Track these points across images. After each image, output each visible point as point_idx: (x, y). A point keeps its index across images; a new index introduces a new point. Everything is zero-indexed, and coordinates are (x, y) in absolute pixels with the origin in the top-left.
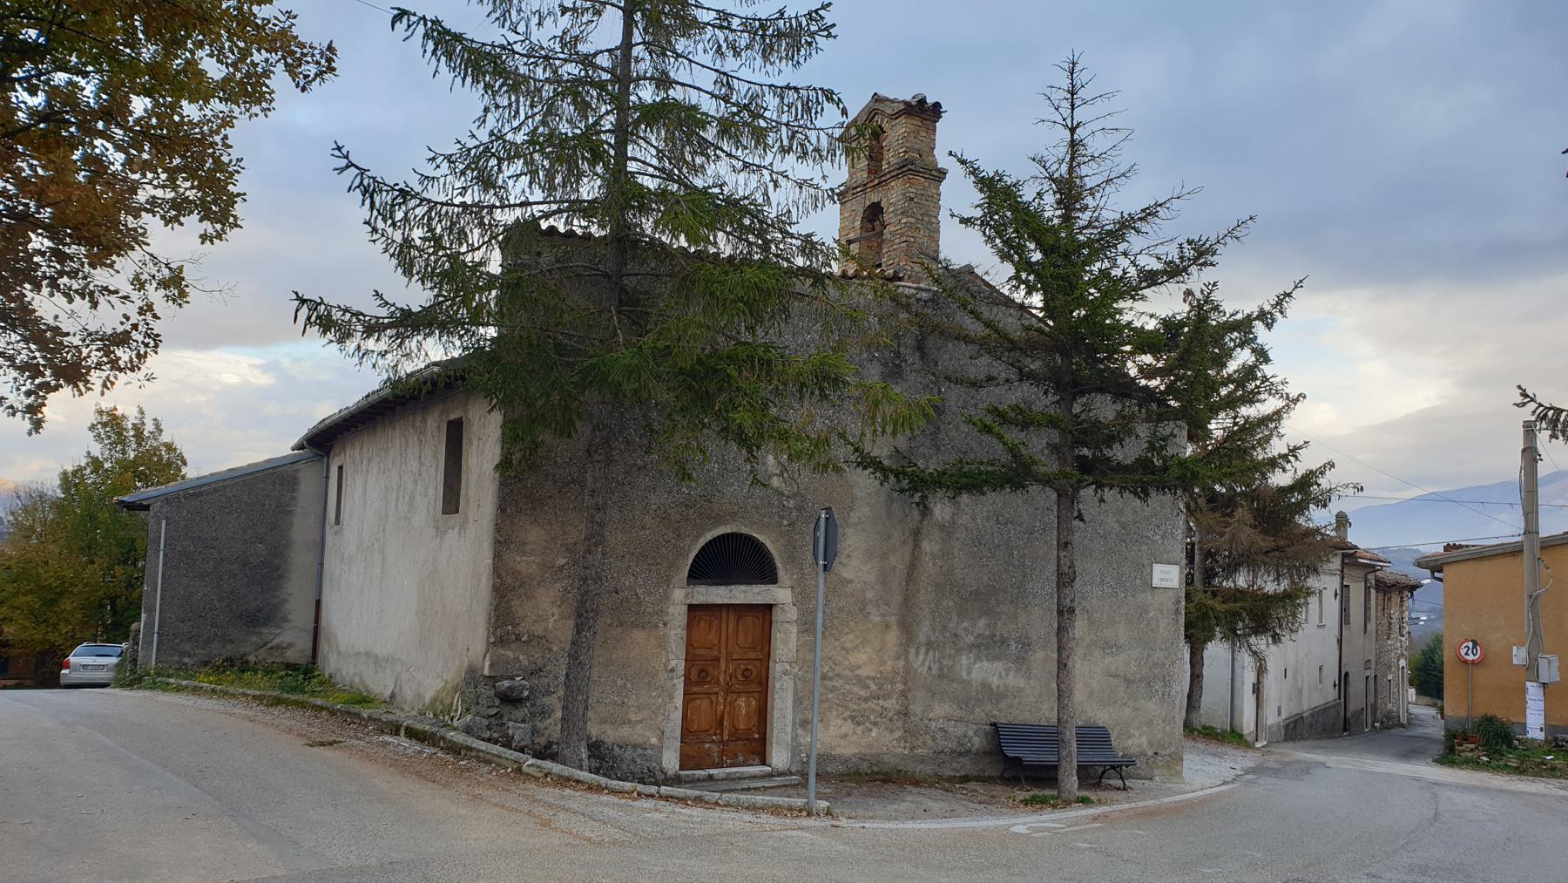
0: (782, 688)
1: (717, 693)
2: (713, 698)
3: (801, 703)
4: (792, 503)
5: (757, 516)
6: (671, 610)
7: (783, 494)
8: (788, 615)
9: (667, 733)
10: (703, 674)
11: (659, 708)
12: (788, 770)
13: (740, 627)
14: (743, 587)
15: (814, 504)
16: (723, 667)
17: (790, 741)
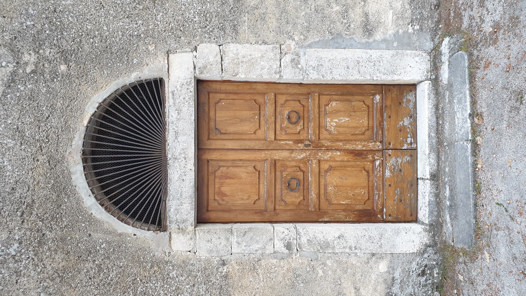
0: (318, 68)
1: (319, 161)
2: (325, 166)
3: (339, 35)
4: (29, 58)
5: (54, 121)
6: (203, 254)
7: (14, 73)
8: (211, 59)
9: (373, 248)
10: (294, 183)
11: (339, 262)
12: (429, 54)
13: (231, 129)
14: (170, 137)
15: (29, 16)
16: (285, 154)
17: (391, 52)
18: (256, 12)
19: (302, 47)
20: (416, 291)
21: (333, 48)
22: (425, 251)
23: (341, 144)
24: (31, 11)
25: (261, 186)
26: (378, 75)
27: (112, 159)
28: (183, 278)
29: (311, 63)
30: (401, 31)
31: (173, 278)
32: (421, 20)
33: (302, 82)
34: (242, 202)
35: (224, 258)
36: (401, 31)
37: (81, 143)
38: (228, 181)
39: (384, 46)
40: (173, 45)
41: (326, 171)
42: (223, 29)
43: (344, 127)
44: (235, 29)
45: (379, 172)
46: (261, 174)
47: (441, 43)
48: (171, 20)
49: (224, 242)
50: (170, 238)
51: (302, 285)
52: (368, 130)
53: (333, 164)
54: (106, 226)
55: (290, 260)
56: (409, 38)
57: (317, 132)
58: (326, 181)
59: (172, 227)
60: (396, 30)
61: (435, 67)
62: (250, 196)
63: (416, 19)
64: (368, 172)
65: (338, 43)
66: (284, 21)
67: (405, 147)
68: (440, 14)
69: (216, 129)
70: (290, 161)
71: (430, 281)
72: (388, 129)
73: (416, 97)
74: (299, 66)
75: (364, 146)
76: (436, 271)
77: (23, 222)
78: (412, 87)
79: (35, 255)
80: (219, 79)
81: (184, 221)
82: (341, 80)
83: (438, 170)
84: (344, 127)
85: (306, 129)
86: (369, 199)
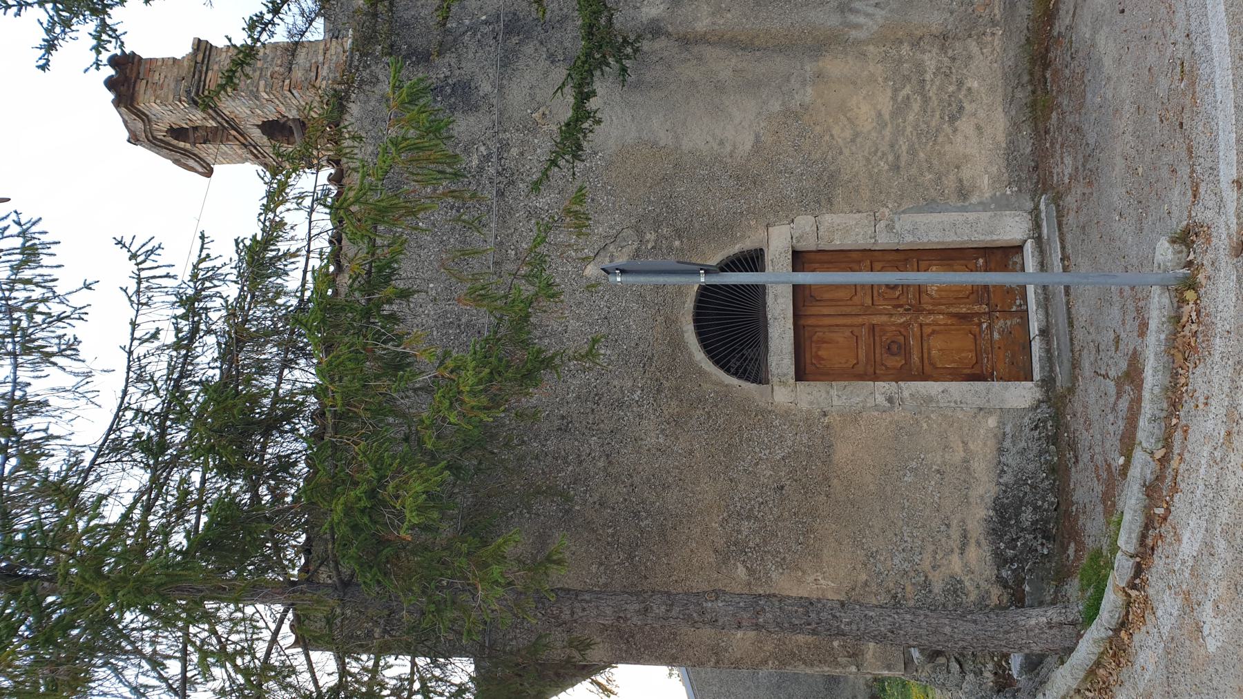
0: (912, 232)
2: (927, 330)
6: (804, 406)
7: (638, 250)
8: (808, 229)
9: (980, 403)
10: (894, 347)
12: (1030, 213)
16: (884, 319)
17: (989, 214)
18: (850, 185)
19: (895, 213)
20: (1030, 445)
21: (927, 213)
22: (1037, 407)
23: (943, 307)
24: (652, 198)
25: (860, 351)
26: (976, 235)
27: (718, 325)
28: (786, 427)
29: (906, 227)
30: (998, 194)
31: (776, 427)
32: (1019, 182)
33: (898, 247)
34: (840, 366)
35: (824, 410)
36: (998, 194)
37: (692, 305)
38: (825, 345)
39: (981, 208)
40: (772, 219)
41: (929, 335)
42: (818, 202)
43: (946, 291)
44: (829, 201)
45: (987, 334)
46: (859, 338)
47: (1039, 201)
48: (770, 197)
49: (824, 395)
50: (772, 389)
51: (906, 437)
52: (972, 293)
53: (937, 328)
54: (714, 378)
55: (892, 413)
56: (1007, 200)
57: (918, 296)
58: (929, 345)
59: (775, 380)
60: (993, 193)
61: (1037, 225)
62: (848, 360)
63: (1014, 181)
64: (975, 336)
65: (932, 208)
66: (877, 191)
67: (1014, 309)
68: (1038, 175)
69: (811, 296)
70: (889, 326)
71: (1043, 435)
72: (994, 291)
73: (1023, 259)
74: (895, 231)
75: (968, 309)
76: (1050, 423)
77: (645, 372)
78: (1019, 248)
79: (655, 401)
80: (814, 248)
81: (785, 375)
82: (938, 243)
83: (1047, 326)
84: (946, 291)
85: (905, 294)
86: (977, 362)
